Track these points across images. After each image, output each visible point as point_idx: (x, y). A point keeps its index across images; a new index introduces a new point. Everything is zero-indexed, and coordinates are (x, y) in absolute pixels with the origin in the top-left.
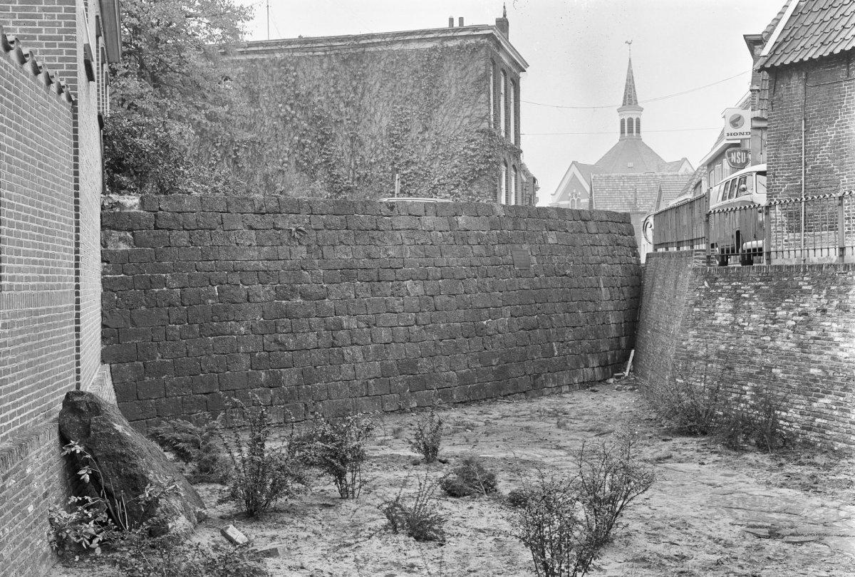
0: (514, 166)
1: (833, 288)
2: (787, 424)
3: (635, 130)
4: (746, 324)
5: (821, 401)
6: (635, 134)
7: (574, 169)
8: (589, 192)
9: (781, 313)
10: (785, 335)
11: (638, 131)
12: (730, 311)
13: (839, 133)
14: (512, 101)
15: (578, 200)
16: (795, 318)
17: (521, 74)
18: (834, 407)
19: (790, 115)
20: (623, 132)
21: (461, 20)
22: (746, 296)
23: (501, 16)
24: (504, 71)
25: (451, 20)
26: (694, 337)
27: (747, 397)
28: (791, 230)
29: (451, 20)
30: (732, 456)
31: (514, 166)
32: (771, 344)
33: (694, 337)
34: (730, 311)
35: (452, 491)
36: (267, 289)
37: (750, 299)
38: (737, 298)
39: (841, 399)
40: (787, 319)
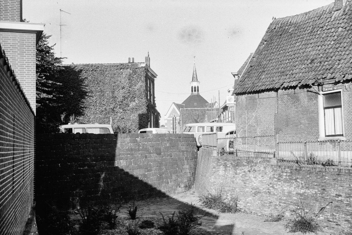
0: (152, 112)
1: (252, 164)
2: (240, 205)
3: (197, 91)
4: (228, 175)
5: (249, 198)
6: (197, 92)
7: (173, 105)
8: (179, 115)
9: (238, 172)
10: (239, 178)
11: (198, 91)
12: (224, 170)
13: (256, 115)
14: (152, 88)
15: (175, 118)
16: (242, 173)
17: (155, 79)
18: (252, 200)
19: (242, 108)
20: (192, 91)
21: (133, 59)
22: (229, 166)
23: (147, 56)
24: (149, 79)
25: (130, 59)
26: (213, 178)
27: (229, 197)
28: (243, 144)
29: (130, 59)
30: (216, 215)
31: (152, 112)
32: (235, 181)
33: (213, 178)
34: (224, 170)
35: (142, 227)
36: (76, 164)
37: (229, 167)
38: (225, 166)
39: (254, 198)
40: (240, 173)
